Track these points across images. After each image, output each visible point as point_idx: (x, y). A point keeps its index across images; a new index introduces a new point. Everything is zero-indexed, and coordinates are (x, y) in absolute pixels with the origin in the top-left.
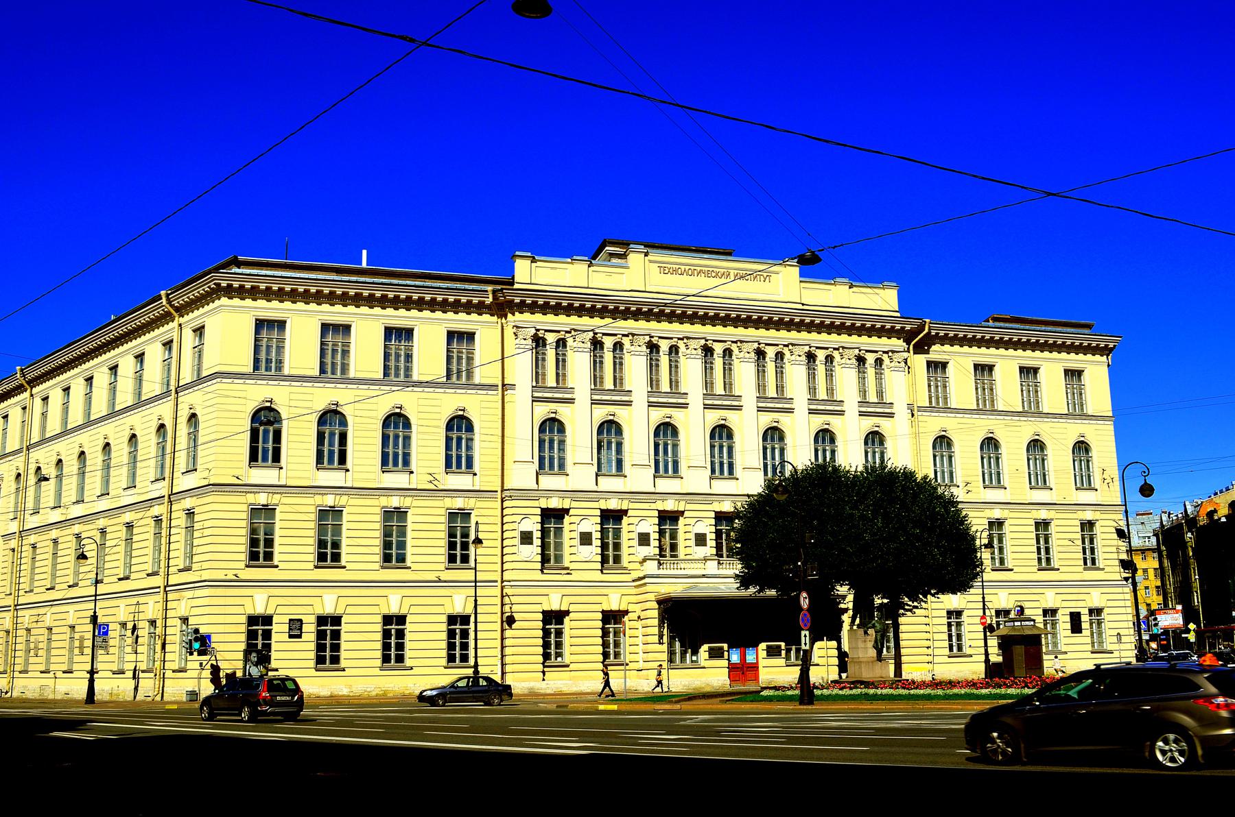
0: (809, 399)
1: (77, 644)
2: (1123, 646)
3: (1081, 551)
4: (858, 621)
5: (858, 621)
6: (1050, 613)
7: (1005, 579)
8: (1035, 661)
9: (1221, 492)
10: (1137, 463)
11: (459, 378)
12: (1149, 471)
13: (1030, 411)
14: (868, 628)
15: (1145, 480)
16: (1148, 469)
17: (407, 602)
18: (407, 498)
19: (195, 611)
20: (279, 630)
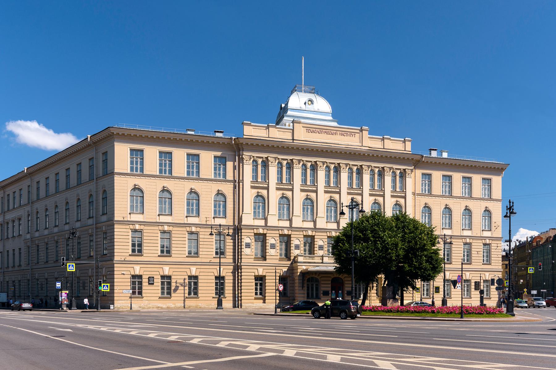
0: (369, 189)
1: (81, 285)
3: (482, 256)
4: (387, 282)
5: (387, 282)
7: (286, 263)
9: (544, 233)
11: (137, 171)
13: (445, 195)
17: (451, 275)
18: (142, 226)
19: (174, 273)
20: (145, 281)
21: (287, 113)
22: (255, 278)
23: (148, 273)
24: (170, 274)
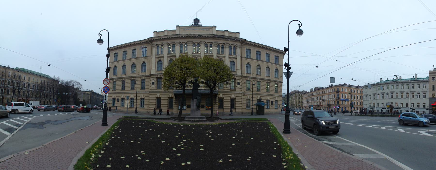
2: (280, 108)
6: (268, 101)
8: (425, 113)
10: (297, 20)
12: (302, 25)
14: (194, 99)
15: (300, 28)
16: (301, 24)
19: (146, 97)
20: (116, 100)
21: (287, 48)
22: (231, 99)
23: (271, 99)
24: (124, 97)
